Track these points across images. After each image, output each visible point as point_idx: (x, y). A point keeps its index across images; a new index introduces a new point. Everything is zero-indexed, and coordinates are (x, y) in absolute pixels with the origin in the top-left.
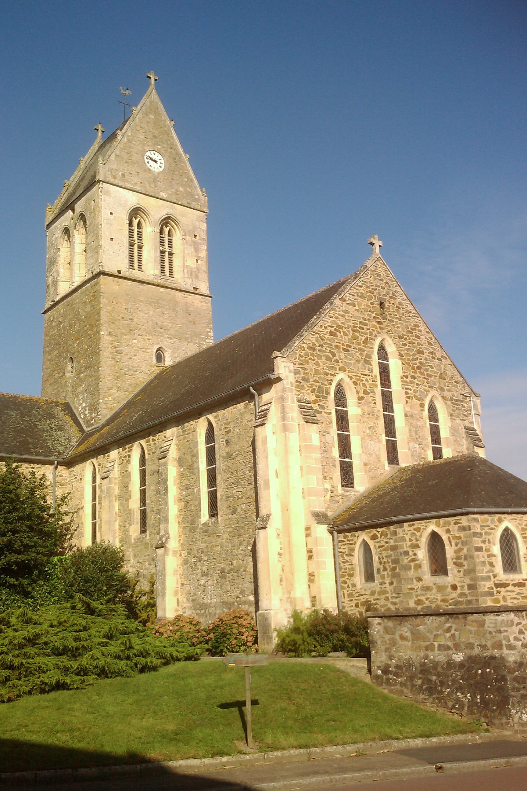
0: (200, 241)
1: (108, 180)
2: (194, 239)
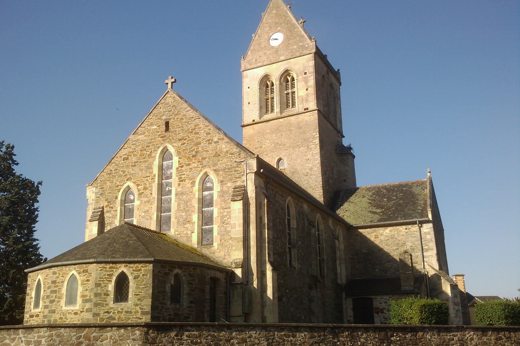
0: (309, 75)
1: (247, 68)
2: (304, 76)
